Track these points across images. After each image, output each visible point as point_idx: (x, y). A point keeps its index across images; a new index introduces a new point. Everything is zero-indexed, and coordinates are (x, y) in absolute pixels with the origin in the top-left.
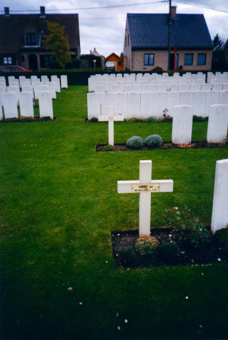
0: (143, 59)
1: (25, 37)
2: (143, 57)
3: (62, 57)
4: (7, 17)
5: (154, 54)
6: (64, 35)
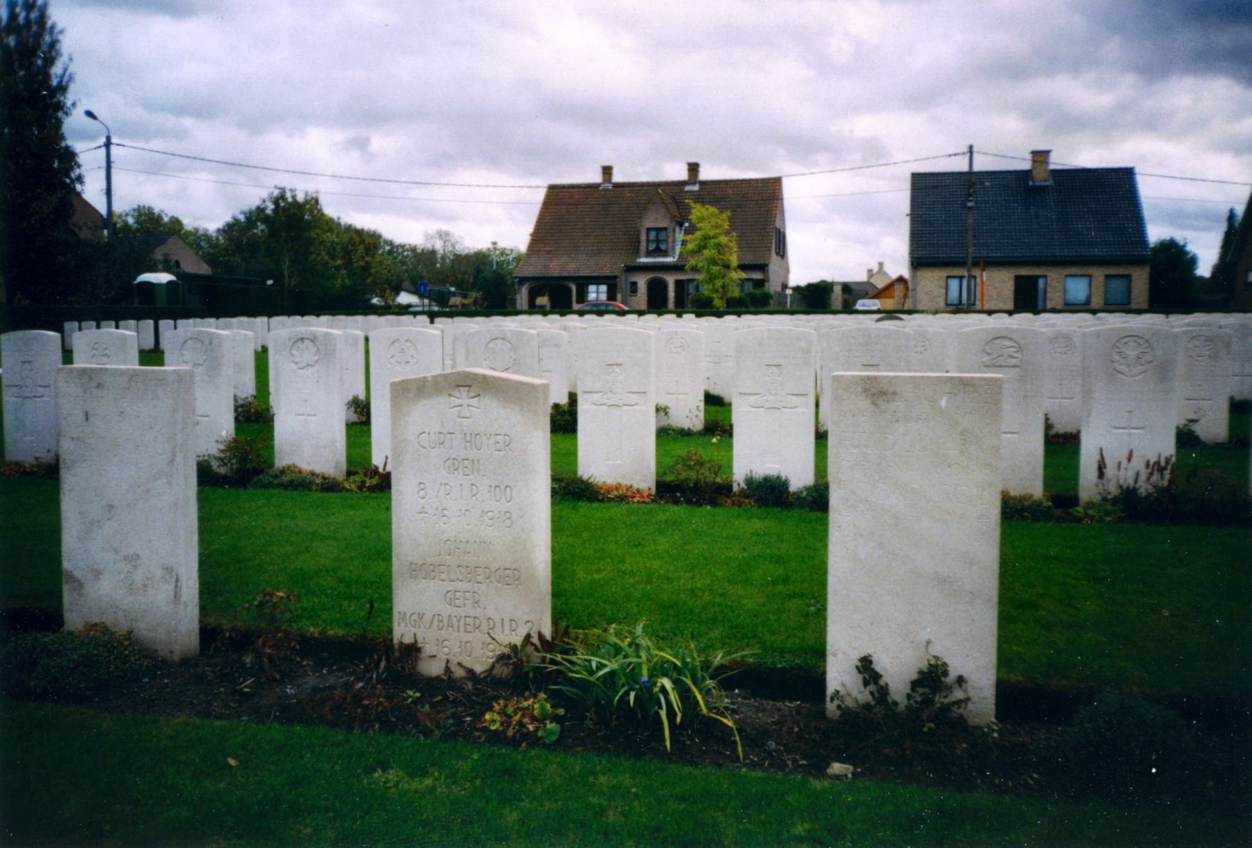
0: (944, 291)
1: (643, 238)
2: (943, 284)
3: (719, 283)
4: (606, 190)
5: (1090, 276)
6: (727, 233)
